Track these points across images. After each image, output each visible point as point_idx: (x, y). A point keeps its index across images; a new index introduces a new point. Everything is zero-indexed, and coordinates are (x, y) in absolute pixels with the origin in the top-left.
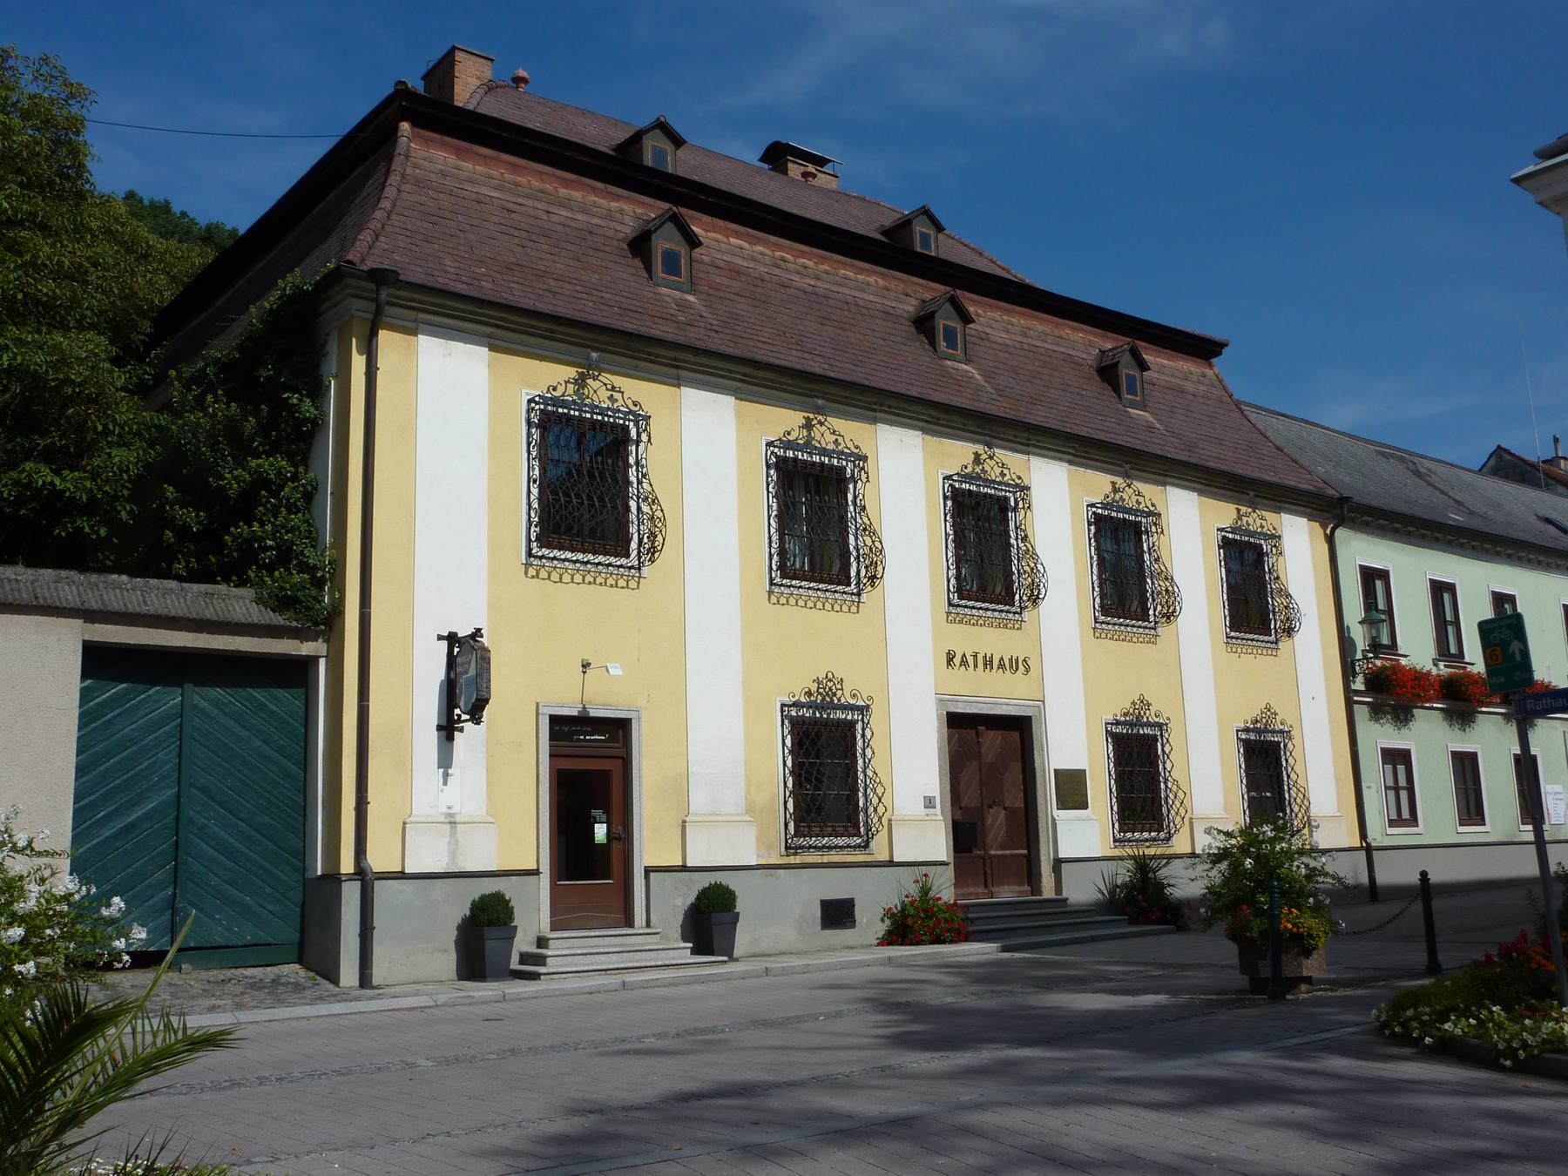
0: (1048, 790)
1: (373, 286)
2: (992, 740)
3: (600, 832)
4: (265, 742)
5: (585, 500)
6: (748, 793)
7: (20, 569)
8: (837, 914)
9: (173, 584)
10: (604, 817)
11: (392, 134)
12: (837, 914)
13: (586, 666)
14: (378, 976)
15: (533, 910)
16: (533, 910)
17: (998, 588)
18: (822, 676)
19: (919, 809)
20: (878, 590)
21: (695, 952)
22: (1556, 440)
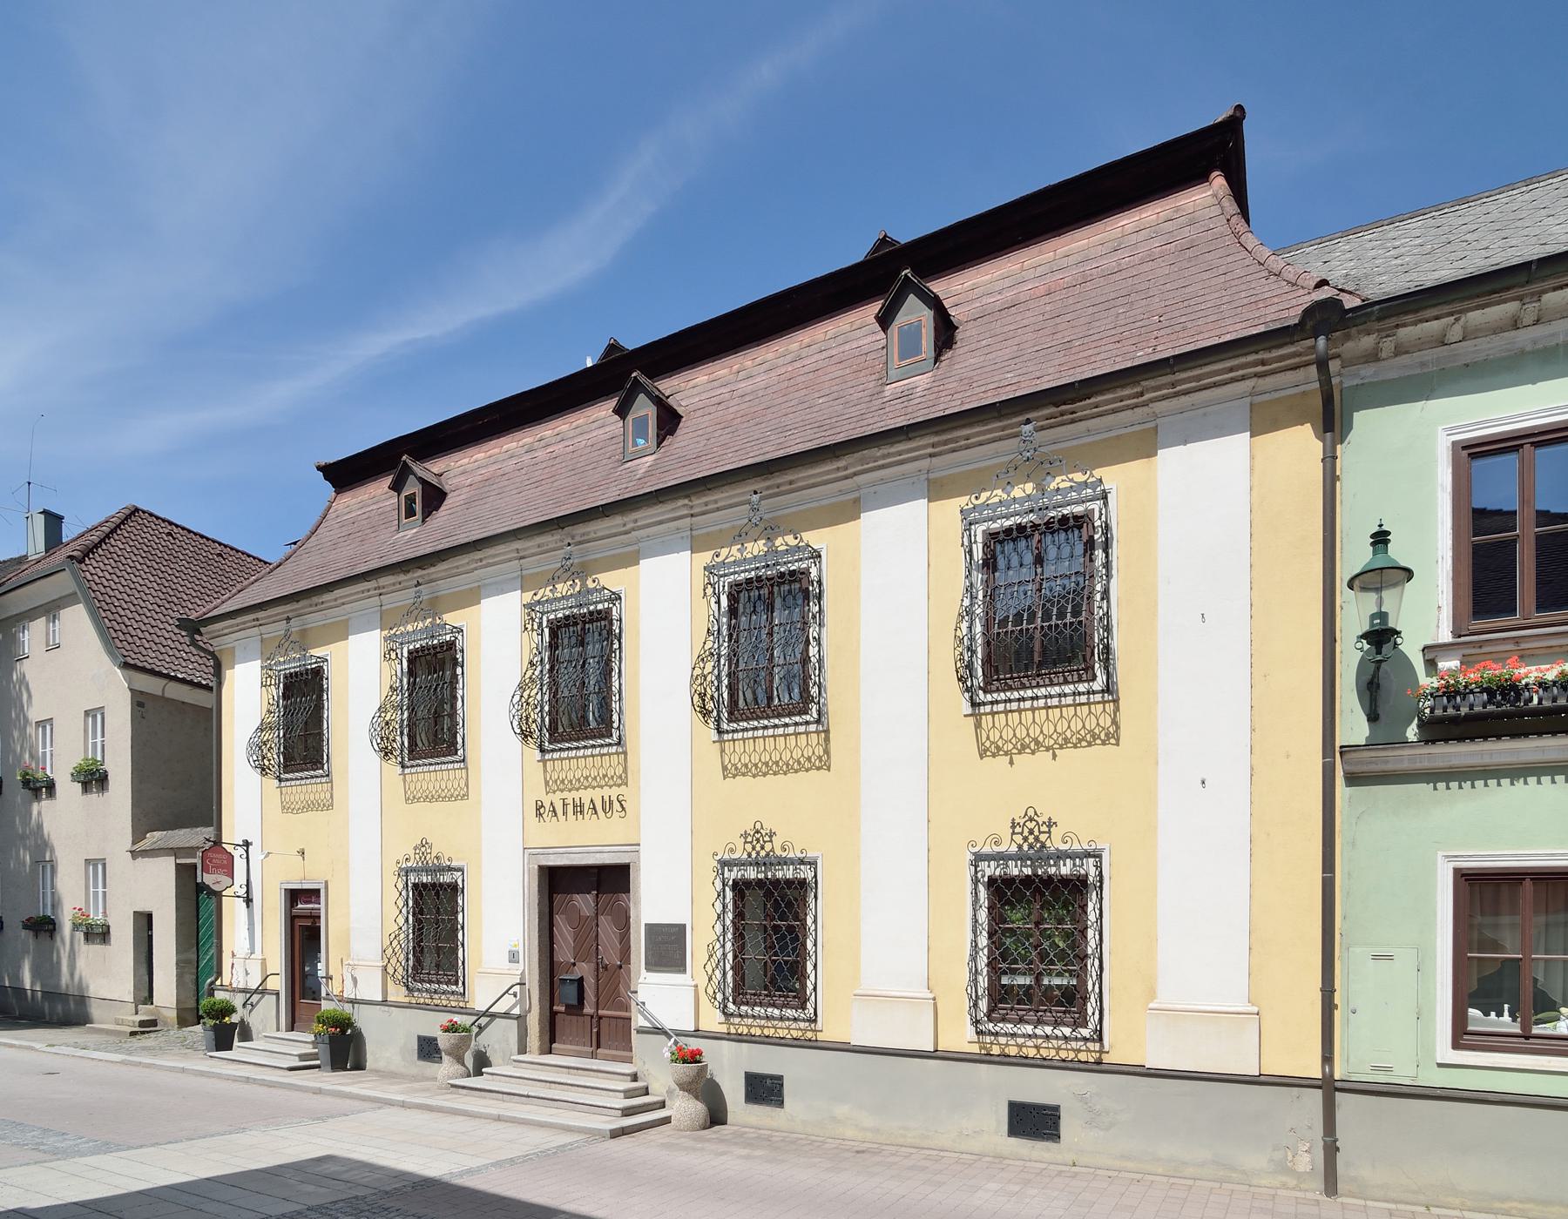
8: (1034, 1121)
18: (1018, 815)
19: (505, 964)
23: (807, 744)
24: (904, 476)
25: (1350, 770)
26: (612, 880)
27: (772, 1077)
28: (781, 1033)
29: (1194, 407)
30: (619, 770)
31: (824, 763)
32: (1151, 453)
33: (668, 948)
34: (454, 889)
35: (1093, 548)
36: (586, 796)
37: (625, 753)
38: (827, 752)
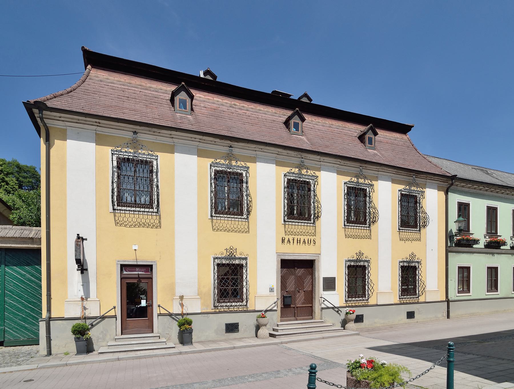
0: (320, 284)
3: (143, 303)
5: (135, 188)
8: (232, 328)
9: (28, 227)
12: (232, 328)
17: (306, 216)
18: (358, 252)
19: (267, 292)
20: (425, 229)
23: (152, 219)
24: (387, 176)
25: (448, 251)
26: (309, 265)
27: (361, 315)
28: (360, 304)
29: (431, 183)
30: (313, 231)
31: (370, 237)
33: (330, 284)
34: (364, 268)
35: (243, 183)
36: (302, 238)
37: (315, 227)
38: (370, 235)
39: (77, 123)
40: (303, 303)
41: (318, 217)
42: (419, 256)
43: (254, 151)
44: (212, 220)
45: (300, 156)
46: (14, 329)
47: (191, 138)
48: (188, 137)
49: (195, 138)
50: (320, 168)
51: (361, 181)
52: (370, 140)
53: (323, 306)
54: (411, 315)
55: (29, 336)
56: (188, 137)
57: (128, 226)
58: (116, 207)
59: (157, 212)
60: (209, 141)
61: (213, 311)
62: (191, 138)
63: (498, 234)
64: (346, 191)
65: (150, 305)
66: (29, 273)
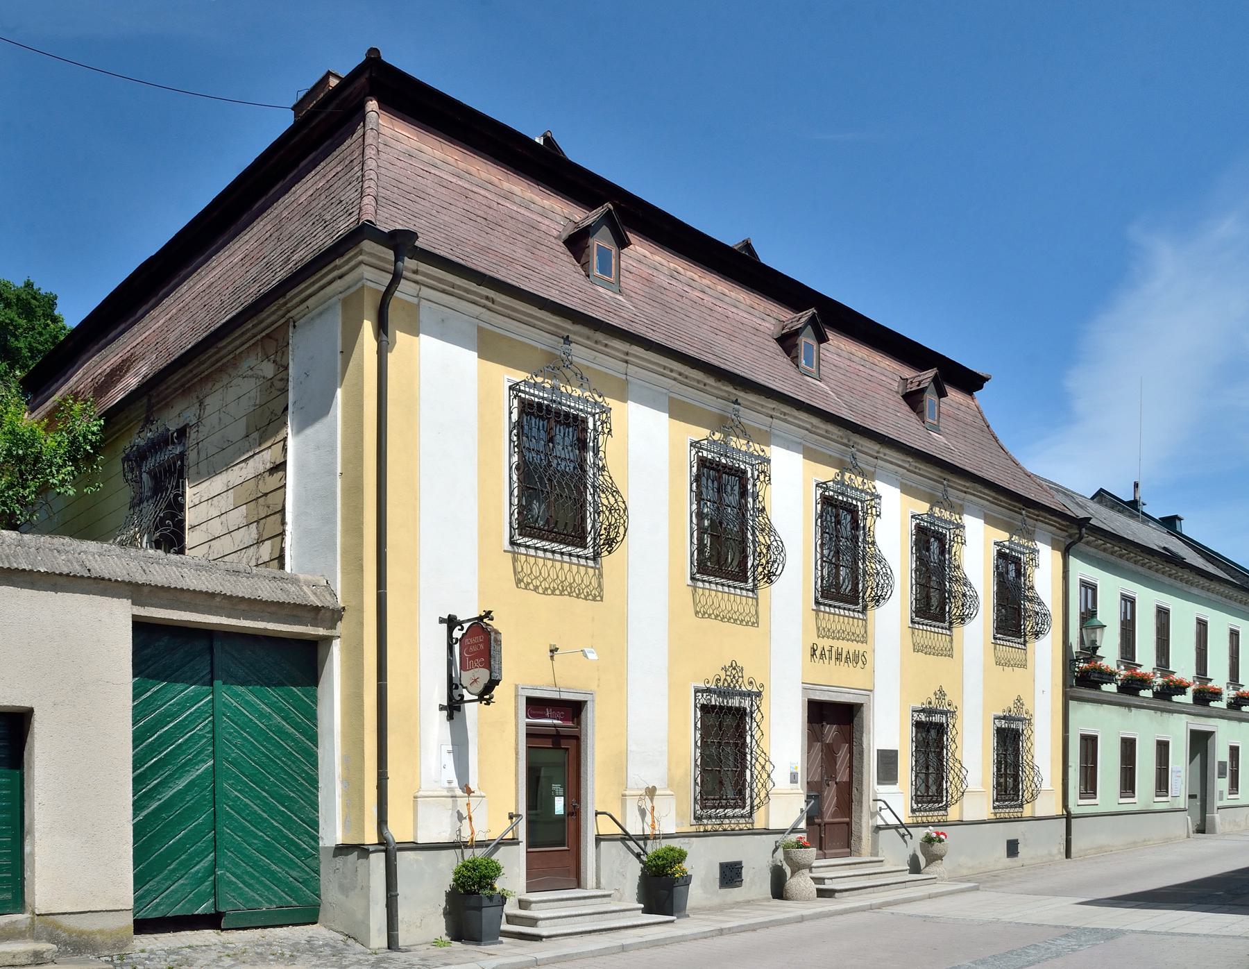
1: (390, 255)
2: (729, 721)
3: (559, 806)
4: (283, 718)
6: (669, 769)
7: (67, 540)
10: (561, 791)
11: (358, 114)
13: (553, 651)
14: (403, 939)
15: (513, 874)
16: (513, 874)
21: (647, 911)
22: (1136, 485)
32: (625, 401)
39: (443, 291)
40: (834, 815)
41: (610, 542)
42: (751, 673)
43: (767, 415)
44: (695, 587)
45: (845, 441)
46: (246, 878)
47: (665, 368)
48: (658, 365)
49: (672, 371)
50: (874, 473)
51: (738, 443)
52: (604, 254)
53: (880, 822)
54: (1012, 848)
55: (281, 898)
56: (658, 365)
57: (557, 592)
58: (516, 537)
59: (753, 591)
60: (694, 379)
61: (693, 829)
62: (665, 368)
63: (1137, 662)
64: (515, 417)
65: (575, 810)
66: (279, 710)
